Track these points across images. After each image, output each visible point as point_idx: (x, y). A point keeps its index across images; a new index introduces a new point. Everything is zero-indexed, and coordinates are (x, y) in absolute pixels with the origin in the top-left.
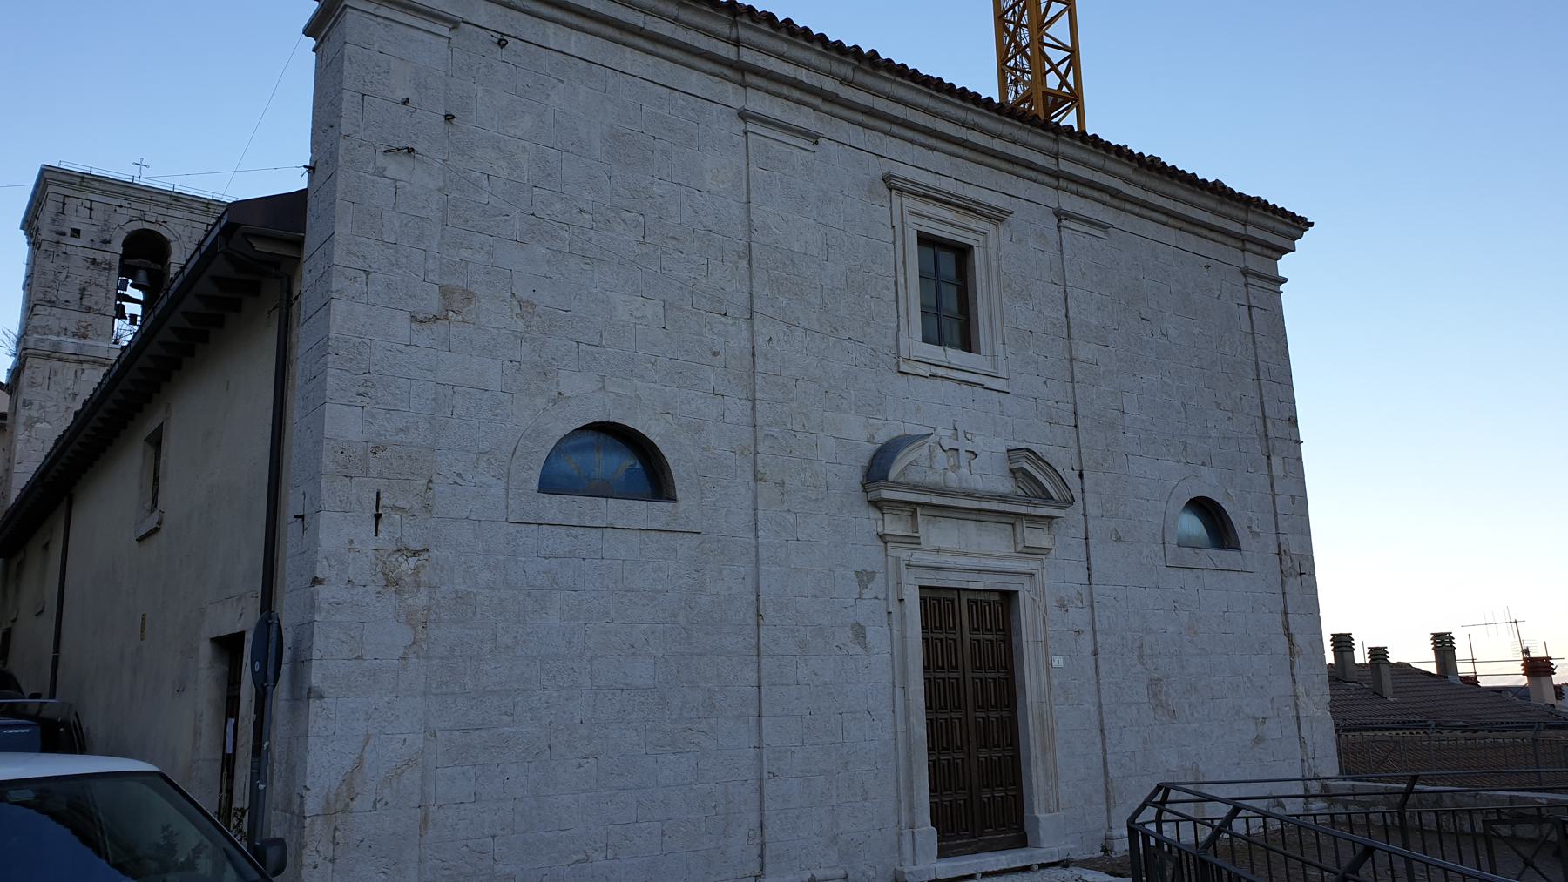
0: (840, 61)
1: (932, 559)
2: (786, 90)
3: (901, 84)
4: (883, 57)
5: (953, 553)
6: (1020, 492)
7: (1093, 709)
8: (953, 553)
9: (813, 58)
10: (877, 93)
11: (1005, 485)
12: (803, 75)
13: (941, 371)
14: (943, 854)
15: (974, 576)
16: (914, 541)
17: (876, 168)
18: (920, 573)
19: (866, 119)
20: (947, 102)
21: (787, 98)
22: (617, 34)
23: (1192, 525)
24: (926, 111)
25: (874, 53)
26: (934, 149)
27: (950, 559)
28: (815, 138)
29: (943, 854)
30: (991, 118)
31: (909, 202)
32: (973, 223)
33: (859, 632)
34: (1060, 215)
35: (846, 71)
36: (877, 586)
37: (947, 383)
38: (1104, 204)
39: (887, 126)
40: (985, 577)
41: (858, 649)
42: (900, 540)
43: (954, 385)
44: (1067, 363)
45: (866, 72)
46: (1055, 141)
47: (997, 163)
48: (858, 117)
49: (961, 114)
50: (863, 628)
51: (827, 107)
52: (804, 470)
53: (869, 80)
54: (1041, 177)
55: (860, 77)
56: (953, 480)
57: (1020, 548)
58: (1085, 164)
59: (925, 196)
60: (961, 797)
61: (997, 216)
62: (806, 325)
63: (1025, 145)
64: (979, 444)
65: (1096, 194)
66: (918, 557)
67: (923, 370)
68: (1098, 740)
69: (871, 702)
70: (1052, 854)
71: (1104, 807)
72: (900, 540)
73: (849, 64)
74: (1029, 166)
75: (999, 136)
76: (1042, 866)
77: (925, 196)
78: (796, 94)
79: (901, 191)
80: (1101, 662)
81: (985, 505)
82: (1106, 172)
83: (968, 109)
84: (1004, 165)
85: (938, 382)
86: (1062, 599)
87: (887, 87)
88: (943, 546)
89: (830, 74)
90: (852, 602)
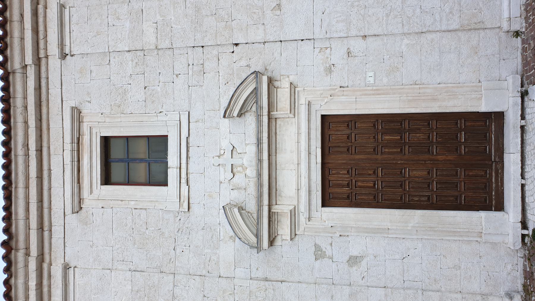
0: (16, 263)
1: (304, 193)
2: (45, 289)
3: (16, 214)
4: (4, 214)
5: (299, 176)
6: (254, 109)
7: (406, 41)
8: (299, 176)
9: (21, 281)
10: (28, 227)
11: (250, 119)
12: (33, 284)
13: (183, 181)
14: (500, 207)
15: (313, 157)
16: (293, 214)
17: (72, 219)
18: (313, 208)
19: (46, 228)
20: (17, 174)
21: (50, 286)
22: (44, 104)
23: (334, 298)
24: (27, 187)
25: (4, 219)
26: (50, 170)
27: (303, 178)
28: (66, 268)
29: (500, 207)
30: (16, 135)
31: (85, 193)
32: (86, 139)
33: (353, 261)
34: (63, 56)
35: (20, 255)
36: (324, 246)
37: (190, 171)
38: (46, 8)
39: (46, 211)
40: (313, 148)
41: (364, 263)
42: (294, 225)
43: (191, 161)
44: (160, 52)
45: (17, 241)
46: (14, 72)
47: (44, 117)
48: (46, 234)
49: (21, 160)
50: (350, 258)
51: (47, 257)
52: (257, 297)
53: (21, 238)
54: (43, 75)
55: (21, 244)
56: (251, 172)
57: (291, 116)
58: (22, 39)
59: (79, 182)
60: (462, 173)
61: (77, 115)
62: (171, 285)
63: (25, 98)
64: (225, 144)
65: (41, 20)
66: (303, 208)
67: (184, 188)
68: (430, 36)
69: (397, 257)
70: (515, 104)
71: (482, 33)
72: (294, 225)
73: (16, 256)
74: (38, 88)
75: (26, 122)
76: (523, 117)
77: (79, 182)
78: (45, 282)
79: (80, 201)
80: (371, 32)
81: (265, 135)
82: (22, 16)
83: (16, 156)
84: (44, 110)
85: (191, 176)
86: (325, 70)
87: (21, 224)
88: (294, 187)
89: (26, 266)
90: (334, 265)
